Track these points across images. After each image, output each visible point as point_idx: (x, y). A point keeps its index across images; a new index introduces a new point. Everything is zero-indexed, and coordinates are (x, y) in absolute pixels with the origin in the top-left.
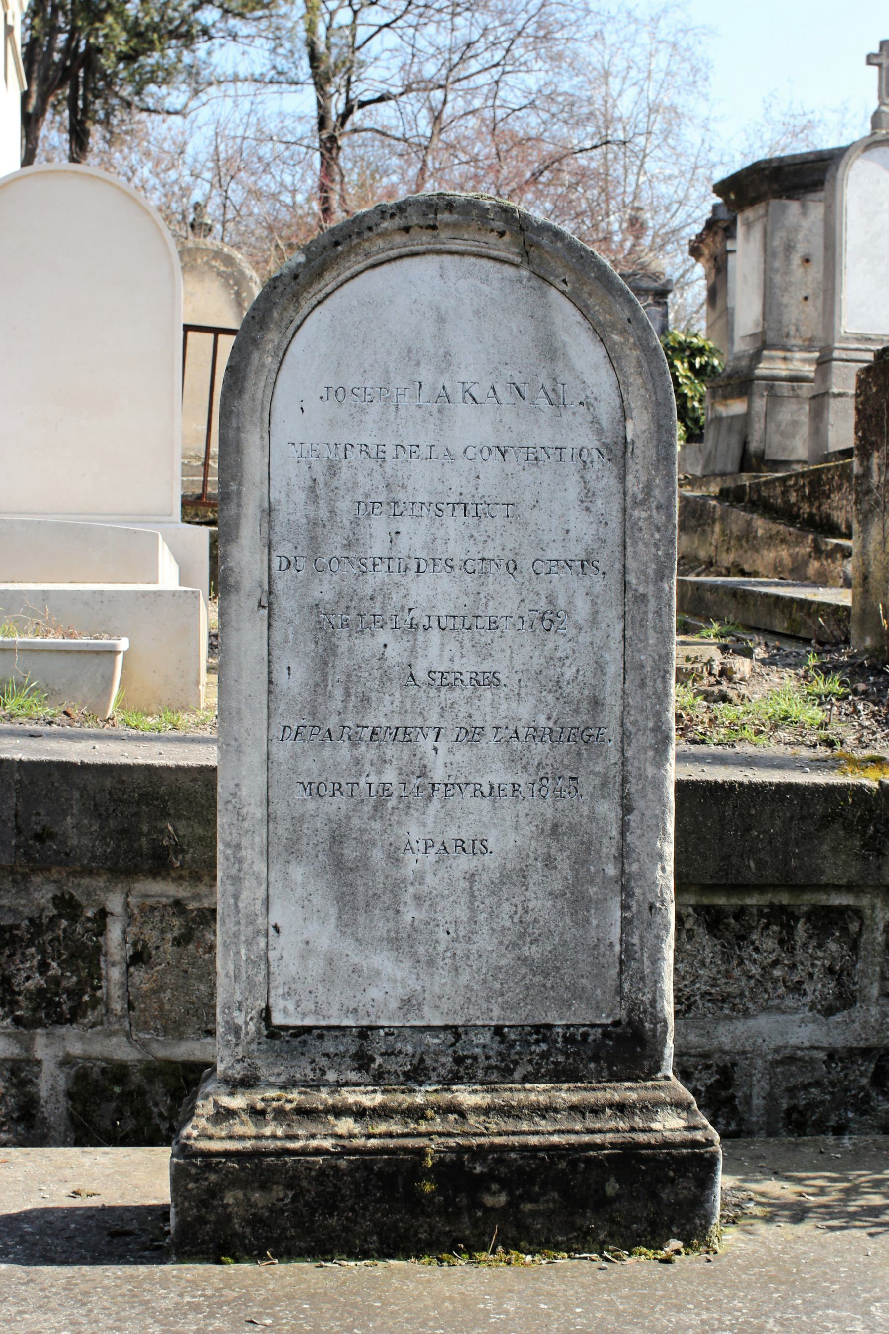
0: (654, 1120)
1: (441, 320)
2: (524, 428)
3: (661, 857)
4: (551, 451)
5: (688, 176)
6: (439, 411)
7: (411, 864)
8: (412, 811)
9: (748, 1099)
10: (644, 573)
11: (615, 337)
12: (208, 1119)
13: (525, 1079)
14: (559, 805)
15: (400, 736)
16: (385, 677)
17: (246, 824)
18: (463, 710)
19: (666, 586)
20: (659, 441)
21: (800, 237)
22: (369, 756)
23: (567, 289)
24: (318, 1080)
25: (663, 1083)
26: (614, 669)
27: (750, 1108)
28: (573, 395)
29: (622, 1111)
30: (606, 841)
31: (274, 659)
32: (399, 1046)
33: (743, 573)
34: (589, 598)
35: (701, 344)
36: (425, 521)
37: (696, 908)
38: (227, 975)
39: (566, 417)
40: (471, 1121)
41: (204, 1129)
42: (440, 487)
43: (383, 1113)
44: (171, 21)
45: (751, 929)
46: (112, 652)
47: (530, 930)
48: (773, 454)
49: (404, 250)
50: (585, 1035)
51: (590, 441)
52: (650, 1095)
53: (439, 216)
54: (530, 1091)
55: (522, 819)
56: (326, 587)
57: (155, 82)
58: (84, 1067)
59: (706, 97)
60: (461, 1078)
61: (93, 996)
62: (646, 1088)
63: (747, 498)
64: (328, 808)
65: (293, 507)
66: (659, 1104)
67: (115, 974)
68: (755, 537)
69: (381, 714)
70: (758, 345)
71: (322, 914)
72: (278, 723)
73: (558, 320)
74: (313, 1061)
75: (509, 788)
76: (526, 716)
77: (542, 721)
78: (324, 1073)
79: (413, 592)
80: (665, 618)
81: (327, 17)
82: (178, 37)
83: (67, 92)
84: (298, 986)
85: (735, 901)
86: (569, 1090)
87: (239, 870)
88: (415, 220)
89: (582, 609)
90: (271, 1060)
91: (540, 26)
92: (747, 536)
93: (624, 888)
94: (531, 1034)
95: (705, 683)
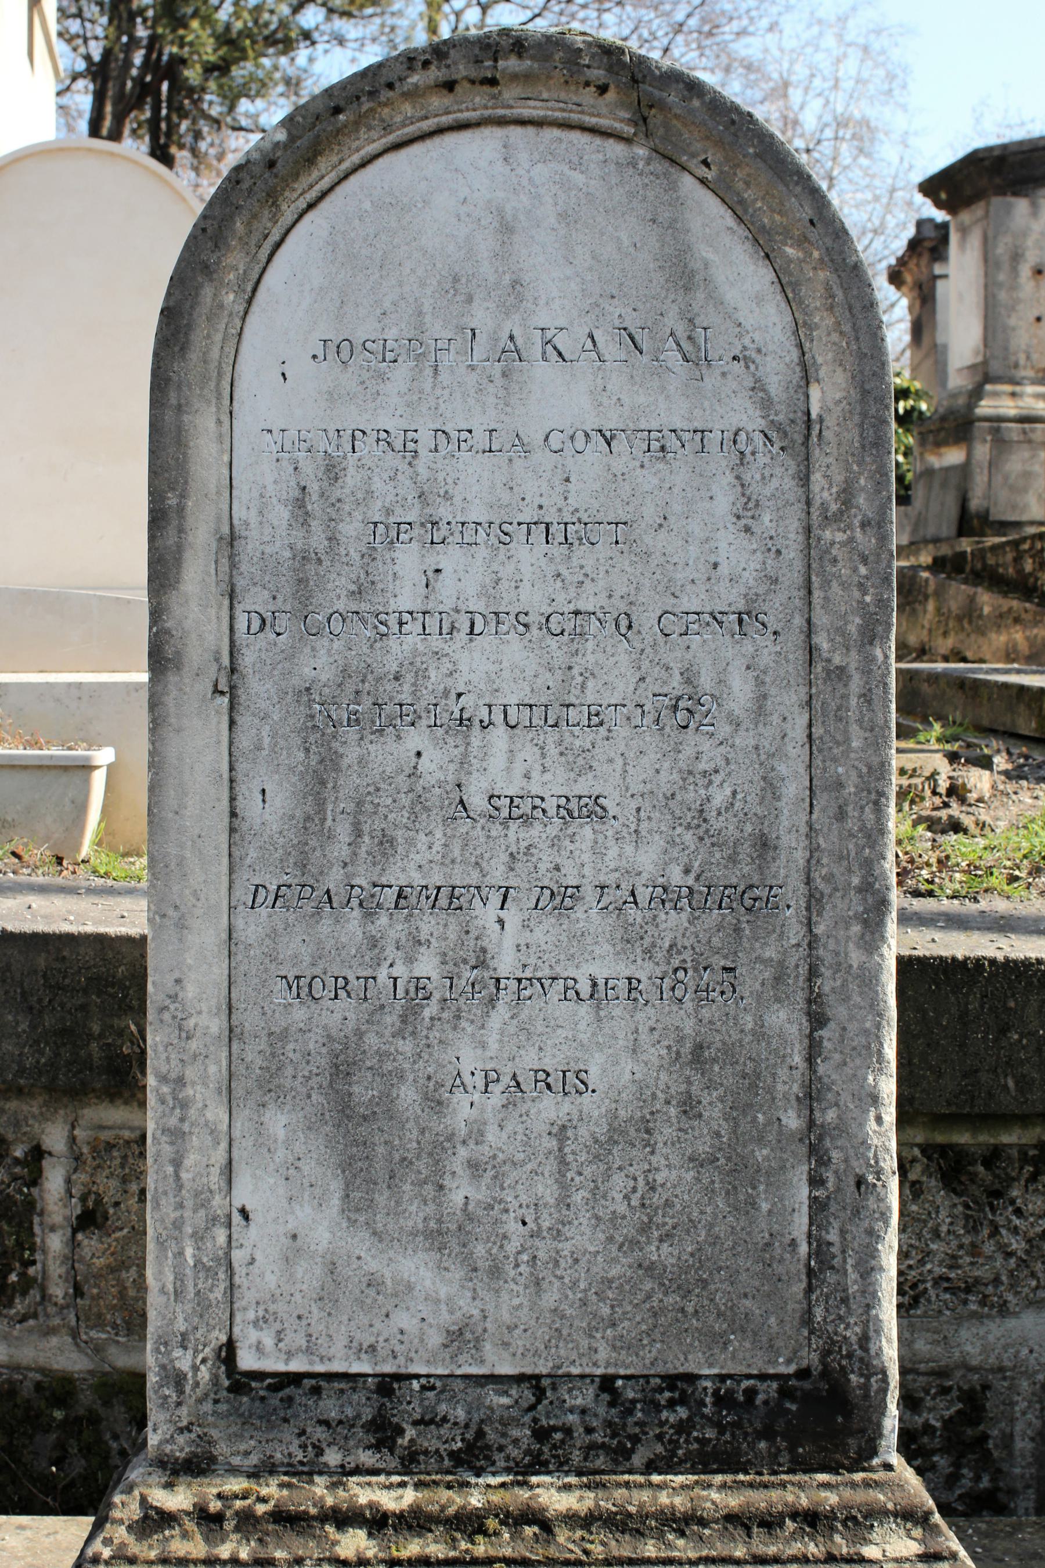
0: (867, 1542)
1: (506, 229)
2: (642, 399)
3: (875, 1099)
4: (686, 436)
5: (884, 201)
6: (504, 375)
7: (462, 1109)
8: (464, 1024)
9: (1008, 1440)
10: (841, 631)
11: (790, 251)
12: (130, 1528)
13: (651, 1467)
14: (705, 1013)
15: (443, 902)
16: (419, 804)
17: (193, 1045)
18: (546, 858)
19: (878, 653)
20: (864, 415)
21: (1030, 243)
22: (393, 934)
23: (710, 175)
24: (311, 1463)
25: (880, 1475)
26: (794, 789)
27: (1011, 1455)
28: (721, 344)
29: (813, 1525)
30: (783, 1073)
31: (239, 777)
32: (443, 1408)
33: (964, 660)
34: (751, 674)
35: (905, 385)
36: (482, 552)
37: (925, 1149)
38: (163, 1291)
39: (712, 380)
40: (561, 1539)
41: (123, 1545)
42: (506, 497)
43: (415, 1522)
44: (267, 25)
45: (1011, 1180)
46: (87, 768)
47: (659, 1219)
48: (1001, 513)
49: (445, 120)
50: (751, 1393)
51: (751, 419)
52: (860, 1496)
53: (501, 63)
54: (660, 1487)
55: (644, 1037)
56: (322, 659)
57: (247, 96)
58: (10, 1381)
59: (904, 108)
60: (545, 1464)
61: (23, 1275)
62: (853, 1485)
63: (968, 568)
64: (326, 1019)
65: (269, 531)
66: (875, 1513)
67: (56, 1243)
68: (980, 616)
69: (412, 865)
70: (978, 378)
71: (318, 1191)
72: (247, 880)
73: (696, 224)
74: (303, 1433)
75: (623, 984)
76: (650, 868)
77: (676, 876)
78: (320, 1452)
79: (463, 667)
80: (877, 704)
81: (452, 18)
82: (275, 43)
83: (148, 114)
84: (280, 1307)
85: (985, 1138)
86: (724, 1486)
87: (182, 1120)
88: (462, 70)
89: (741, 690)
90: (234, 1429)
91: (704, 20)
92: (970, 614)
93: (814, 1150)
94: (661, 1390)
95: (927, 806)
